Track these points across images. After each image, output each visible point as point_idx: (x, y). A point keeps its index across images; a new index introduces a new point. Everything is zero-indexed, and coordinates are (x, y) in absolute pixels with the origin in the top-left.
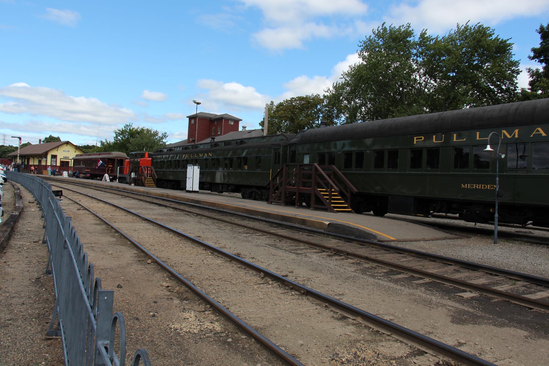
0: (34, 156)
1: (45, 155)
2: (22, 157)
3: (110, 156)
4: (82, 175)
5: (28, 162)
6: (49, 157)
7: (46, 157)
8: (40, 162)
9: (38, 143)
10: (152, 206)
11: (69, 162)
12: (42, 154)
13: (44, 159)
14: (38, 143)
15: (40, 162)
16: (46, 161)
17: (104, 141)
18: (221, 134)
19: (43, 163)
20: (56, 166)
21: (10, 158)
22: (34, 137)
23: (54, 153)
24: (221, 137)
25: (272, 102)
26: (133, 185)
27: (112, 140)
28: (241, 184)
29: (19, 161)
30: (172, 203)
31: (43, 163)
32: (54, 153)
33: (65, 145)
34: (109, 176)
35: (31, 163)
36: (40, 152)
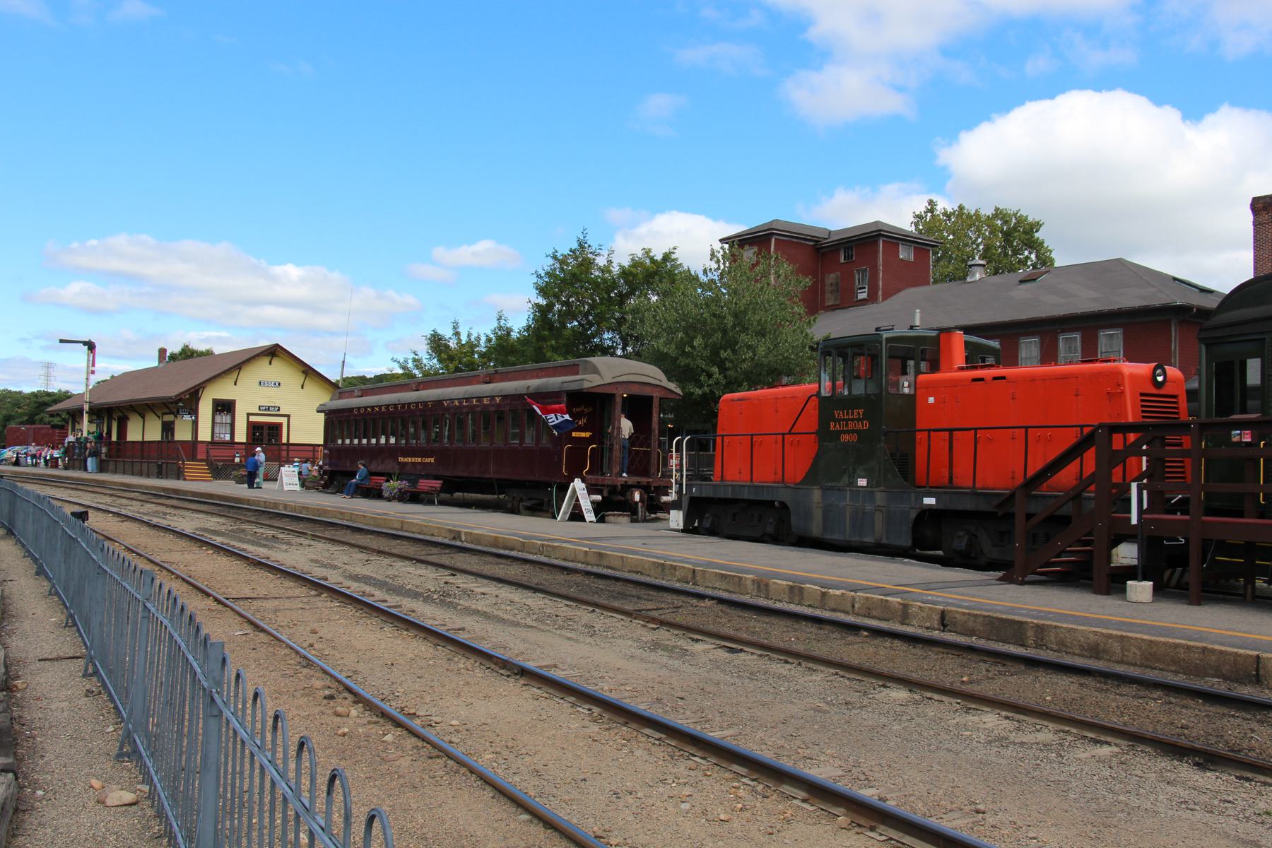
0: (143, 408)
1: (189, 401)
2: (100, 412)
3: (589, 381)
4: (394, 485)
5: (122, 432)
6: (205, 408)
7: (194, 411)
8: (168, 428)
9: (156, 364)
10: (196, 515)
11: (281, 424)
12: (179, 398)
13: (187, 418)
14: (156, 364)
15: (168, 428)
16: (195, 423)
17: (447, 332)
18: (872, 298)
19: (182, 434)
20: (232, 442)
21: (56, 421)
22: (127, 356)
23: (223, 391)
24: (872, 308)
25: (931, 202)
26: (1141, 590)
27: (519, 321)
28: (952, 507)
29: (87, 427)
30: (435, 550)
31: (182, 434)
32: (223, 391)
33: (266, 360)
34: (591, 490)
35: (134, 435)
36: (172, 391)
